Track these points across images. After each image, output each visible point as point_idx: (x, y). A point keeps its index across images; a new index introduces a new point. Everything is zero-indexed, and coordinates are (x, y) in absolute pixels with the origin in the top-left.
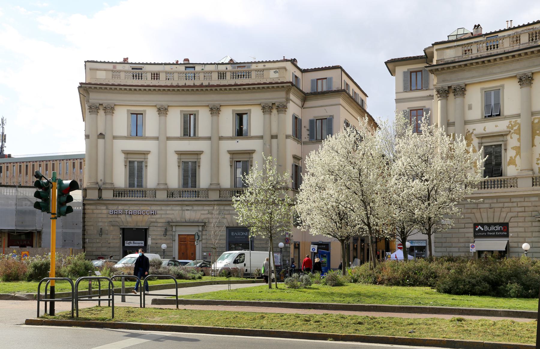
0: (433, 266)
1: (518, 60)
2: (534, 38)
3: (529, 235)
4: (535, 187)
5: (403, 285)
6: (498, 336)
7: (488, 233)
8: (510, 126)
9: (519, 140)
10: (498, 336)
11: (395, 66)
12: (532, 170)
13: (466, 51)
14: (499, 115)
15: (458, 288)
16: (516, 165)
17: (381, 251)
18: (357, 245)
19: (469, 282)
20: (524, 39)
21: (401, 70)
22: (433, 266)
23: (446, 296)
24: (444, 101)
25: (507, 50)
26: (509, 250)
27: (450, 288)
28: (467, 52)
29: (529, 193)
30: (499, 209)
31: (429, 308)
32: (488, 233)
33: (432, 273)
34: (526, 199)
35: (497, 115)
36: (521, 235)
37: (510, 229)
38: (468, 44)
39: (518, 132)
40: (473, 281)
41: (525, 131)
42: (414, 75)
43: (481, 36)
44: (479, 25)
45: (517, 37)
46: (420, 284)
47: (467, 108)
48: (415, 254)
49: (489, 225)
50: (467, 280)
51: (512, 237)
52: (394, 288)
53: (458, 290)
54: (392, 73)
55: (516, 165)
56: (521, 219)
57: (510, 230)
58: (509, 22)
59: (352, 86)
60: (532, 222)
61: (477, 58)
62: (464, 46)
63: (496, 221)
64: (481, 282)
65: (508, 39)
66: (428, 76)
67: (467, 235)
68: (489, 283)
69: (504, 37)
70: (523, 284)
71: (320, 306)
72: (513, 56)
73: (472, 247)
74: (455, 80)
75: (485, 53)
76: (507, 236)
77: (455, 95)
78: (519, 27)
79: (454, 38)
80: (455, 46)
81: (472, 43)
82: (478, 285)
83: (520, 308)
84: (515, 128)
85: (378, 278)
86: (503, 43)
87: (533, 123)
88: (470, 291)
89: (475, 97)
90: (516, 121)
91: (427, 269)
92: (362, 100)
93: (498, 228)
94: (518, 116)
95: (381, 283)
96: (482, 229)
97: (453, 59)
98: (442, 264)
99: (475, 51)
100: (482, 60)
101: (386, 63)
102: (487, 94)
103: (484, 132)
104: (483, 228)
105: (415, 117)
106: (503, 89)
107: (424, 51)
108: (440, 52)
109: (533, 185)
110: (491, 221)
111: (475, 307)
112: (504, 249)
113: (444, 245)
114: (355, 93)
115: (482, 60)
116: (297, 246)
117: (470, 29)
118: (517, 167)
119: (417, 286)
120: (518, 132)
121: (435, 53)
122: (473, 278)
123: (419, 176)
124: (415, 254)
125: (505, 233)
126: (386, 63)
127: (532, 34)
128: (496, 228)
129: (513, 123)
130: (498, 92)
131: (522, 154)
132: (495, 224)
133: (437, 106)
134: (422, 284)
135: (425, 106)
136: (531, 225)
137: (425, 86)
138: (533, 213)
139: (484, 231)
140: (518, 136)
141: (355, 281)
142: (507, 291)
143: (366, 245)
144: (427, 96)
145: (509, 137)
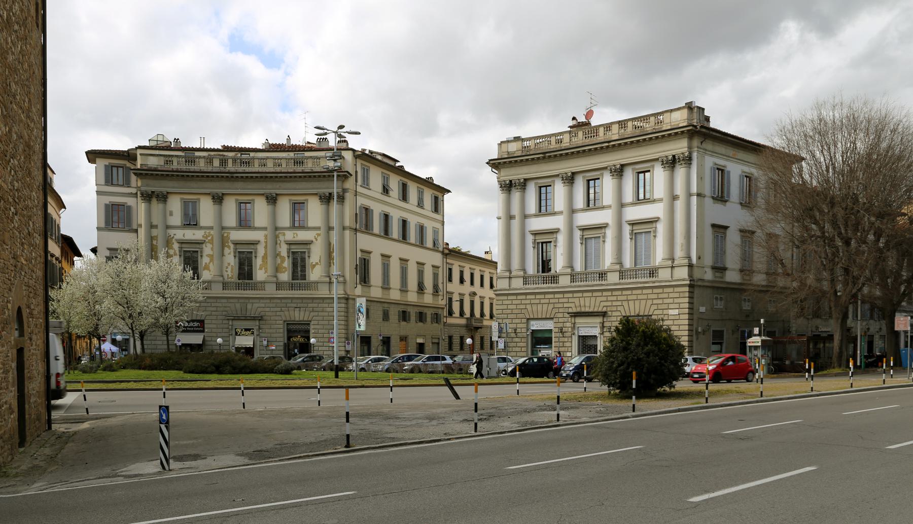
3: (220, 330)
9: (212, 249)
20: (216, 163)
36: (214, 330)
56: (215, 317)
61: (177, 171)
63: (194, 318)
69: (200, 157)
87: (223, 236)
93: (196, 324)
94: (211, 228)
95: (144, 369)
99: (175, 163)
102: (185, 204)
120: (211, 242)
121: (139, 157)
130: (195, 203)
141: (124, 368)
145: (204, 246)
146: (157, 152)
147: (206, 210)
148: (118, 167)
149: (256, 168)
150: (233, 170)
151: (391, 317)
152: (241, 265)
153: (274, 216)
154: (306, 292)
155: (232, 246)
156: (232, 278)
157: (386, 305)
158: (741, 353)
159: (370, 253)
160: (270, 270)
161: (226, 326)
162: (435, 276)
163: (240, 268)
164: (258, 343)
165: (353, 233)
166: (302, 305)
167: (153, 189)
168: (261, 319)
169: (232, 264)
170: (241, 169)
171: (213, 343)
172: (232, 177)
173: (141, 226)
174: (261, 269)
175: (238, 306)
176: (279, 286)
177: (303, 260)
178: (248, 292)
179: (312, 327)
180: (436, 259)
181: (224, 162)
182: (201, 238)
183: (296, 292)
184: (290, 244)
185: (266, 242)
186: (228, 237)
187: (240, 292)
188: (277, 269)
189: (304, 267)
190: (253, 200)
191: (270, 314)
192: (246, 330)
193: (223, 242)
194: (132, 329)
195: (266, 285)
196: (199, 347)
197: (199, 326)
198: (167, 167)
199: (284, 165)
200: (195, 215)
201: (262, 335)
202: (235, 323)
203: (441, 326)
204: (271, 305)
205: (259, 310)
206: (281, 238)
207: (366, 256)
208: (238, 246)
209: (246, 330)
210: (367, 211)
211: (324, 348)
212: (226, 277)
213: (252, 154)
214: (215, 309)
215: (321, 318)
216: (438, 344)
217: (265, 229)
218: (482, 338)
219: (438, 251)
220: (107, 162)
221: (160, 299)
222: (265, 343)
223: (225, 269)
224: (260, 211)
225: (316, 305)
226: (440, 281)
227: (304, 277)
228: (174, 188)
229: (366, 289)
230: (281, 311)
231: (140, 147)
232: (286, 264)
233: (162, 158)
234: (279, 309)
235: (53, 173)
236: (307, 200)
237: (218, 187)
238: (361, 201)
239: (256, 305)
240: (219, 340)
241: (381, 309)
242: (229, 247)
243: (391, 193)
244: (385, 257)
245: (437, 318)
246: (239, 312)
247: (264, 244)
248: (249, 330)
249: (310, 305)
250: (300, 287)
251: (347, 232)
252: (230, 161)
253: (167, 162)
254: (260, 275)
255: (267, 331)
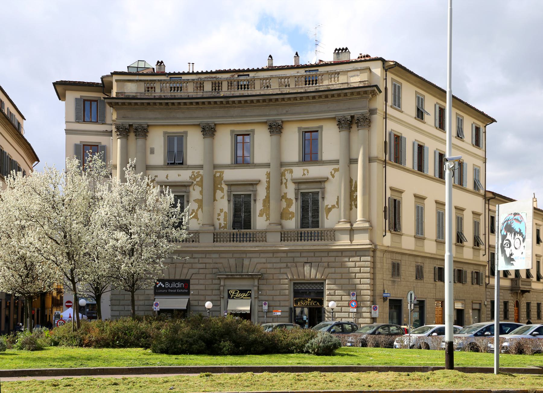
0: (143, 325)
1: (201, 108)
2: (217, 88)
3: (209, 292)
4: (216, 244)
5: (114, 347)
6: (248, 386)
7: (169, 290)
8: (193, 176)
9: (201, 192)
10: (248, 386)
11: (65, 90)
12: (213, 225)
13: (148, 88)
14: (182, 164)
15: (175, 348)
16: (198, 219)
17: (36, 310)
18: (10, 303)
19: (187, 341)
20: (208, 87)
21: (72, 96)
22: (143, 325)
23: (165, 356)
24: (124, 140)
25: (191, 95)
26: (190, 308)
27: (168, 348)
28: (150, 89)
29: (210, 249)
30: (181, 265)
31: (159, 368)
32: (169, 290)
33: (143, 333)
34: (208, 256)
35: (179, 164)
36: (202, 292)
37: (191, 286)
38: (151, 81)
39: (201, 184)
40: (190, 340)
41: (208, 183)
42: (88, 104)
43: (164, 74)
44: (162, 62)
45: (200, 83)
46: (130, 345)
47: (148, 151)
48: (86, 313)
49: (170, 281)
50: (185, 339)
51: (193, 295)
52: (105, 350)
53: (176, 350)
54: (61, 96)
55: (198, 219)
56: (202, 276)
57: (191, 287)
58: (191, 65)
59: (7, 104)
60: (212, 279)
61: (160, 98)
62: (146, 82)
63: (178, 277)
64: (198, 341)
65: (192, 84)
66: (105, 107)
67: (147, 292)
68: (204, 341)
69: (188, 81)
70: (234, 342)
71: (37, 373)
72: (197, 103)
73: (156, 306)
74: (136, 118)
75: (168, 94)
76: (188, 294)
77: (136, 135)
78: (202, 73)
79: (134, 71)
80: (137, 81)
81: (155, 80)
82: (195, 344)
83: (240, 363)
84: (198, 180)
85: (84, 340)
86: (187, 87)
87: (214, 176)
88: (188, 350)
89: (157, 140)
90: (199, 172)
91: (137, 329)
92: (19, 123)
93: (179, 285)
94: (201, 167)
95: (88, 345)
96: (163, 286)
97: (134, 94)
98: (151, 323)
99: (158, 90)
100: (166, 101)
101: (55, 84)
102: (169, 139)
103: (166, 180)
104: (164, 284)
105: (84, 152)
106: (187, 136)
107: (102, 79)
108: (120, 83)
109: (214, 241)
110: (172, 277)
111: (199, 364)
112: (185, 308)
113: (122, 303)
114: (11, 113)
115: (166, 101)
116: (16, 304)
117: (152, 64)
118: (199, 222)
119: (128, 347)
120: (201, 184)
121: (115, 85)
122: (190, 337)
123: (124, 228)
124: (86, 313)
125: (186, 291)
126: (55, 84)
127: (215, 84)
128: (177, 285)
129: (196, 175)
130: (181, 139)
131: (204, 208)
132: (176, 281)
133: (116, 145)
134: (133, 345)
135: (100, 143)
136: (211, 283)
137: (100, 119)
138: (214, 270)
139: (165, 288)
140: (200, 189)
141: (56, 344)
142: (221, 349)
143: (20, 303)
144: (103, 132)
145: (191, 189)
146: (137, 78)
147: (195, 146)
148: (91, 101)
149: (257, 90)
150: (228, 94)
151: (426, 275)
152: (237, 211)
153: (278, 149)
154: (320, 242)
155: (225, 188)
156: (224, 227)
157: (419, 260)
158: (444, 334)
159: (401, 192)
160: (274, 216)
161: (217, 287)
162: (476, 225)
163: (235, 216)
164: (256, 309)
165: (381, 166)
166: (313, 259)
167: (131, 122)
168: (260, 277)
169: (226, 209)
170: (237, 93)
171: (200, 308)
172: (227, 103)
173: (115, 167)
174: (261, 215)
175: (232, 262)
176: (285, 236)
177: (316, 203)
178: (245, 244)
179: (327, 287)
180: (475, 204)
181: (217, 85)
182: (188, 179)
183: (306, 242)
184: (298, 183)
185: (268, 182)
186: (221, 177)
187: (235, 244)
188: (283, 215)
189: (316, 212)
190: (253, 131)
191: (273, 271)
192: (242, 291)
193: (216, 183)
194: (73, 281)
195: (268, 234)
196: (182, 313)
197: (183, 287)
198: (148, 95)
199: (292, 86)
200: (181, 153)
201: (261, 297)
202: (229, 283)
203: (483, 288)
204: (274, 260)
205: (259, 266)
206: (288, 176)
207: (396, 196)
208: (233, 188)
209: (242, 291)
210: (398, 139)
211: (342, 315)
212: (217, 226)
213: (252, 74)
214: (203, 266)
215: (339, 276)
216: (479, 310)
217: (268, 165)
218: (528, 304)
219: (479, 195)
220: (78, 94)
221: (121, 235)
222: (265, 308)
223: (216, 216)
224: (262, 143)
225: (332, 259)
226: (482, 231)
227: (316, 224)
228: (156, 119)
229: (396, 238)
230: (287, 267)
231: (116, 73)
232: (293, 209)
233: (142, 84)
234: (284, 265)
235: (23, 118)
236: (321, 127)
237: (206, 116)
238: (392, 126)
239: (255, 261)
240: (208, 305)
241: (414, 264)
242: (222, 190)
243: (426, 117)
244: (420, 198)
245: (477, 278)
246: (233, 269)
247: (265, 185)
248: (245, 291)
249: (324, 259)
250: (311, 237)
251: (376, 167)
252: (225, 85)
253: (148, 89)
254: (260, 222)
255: (269, 293)
